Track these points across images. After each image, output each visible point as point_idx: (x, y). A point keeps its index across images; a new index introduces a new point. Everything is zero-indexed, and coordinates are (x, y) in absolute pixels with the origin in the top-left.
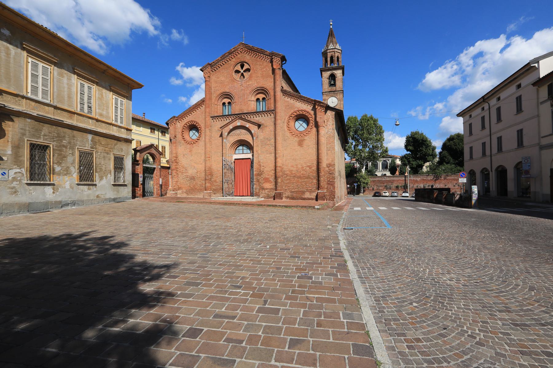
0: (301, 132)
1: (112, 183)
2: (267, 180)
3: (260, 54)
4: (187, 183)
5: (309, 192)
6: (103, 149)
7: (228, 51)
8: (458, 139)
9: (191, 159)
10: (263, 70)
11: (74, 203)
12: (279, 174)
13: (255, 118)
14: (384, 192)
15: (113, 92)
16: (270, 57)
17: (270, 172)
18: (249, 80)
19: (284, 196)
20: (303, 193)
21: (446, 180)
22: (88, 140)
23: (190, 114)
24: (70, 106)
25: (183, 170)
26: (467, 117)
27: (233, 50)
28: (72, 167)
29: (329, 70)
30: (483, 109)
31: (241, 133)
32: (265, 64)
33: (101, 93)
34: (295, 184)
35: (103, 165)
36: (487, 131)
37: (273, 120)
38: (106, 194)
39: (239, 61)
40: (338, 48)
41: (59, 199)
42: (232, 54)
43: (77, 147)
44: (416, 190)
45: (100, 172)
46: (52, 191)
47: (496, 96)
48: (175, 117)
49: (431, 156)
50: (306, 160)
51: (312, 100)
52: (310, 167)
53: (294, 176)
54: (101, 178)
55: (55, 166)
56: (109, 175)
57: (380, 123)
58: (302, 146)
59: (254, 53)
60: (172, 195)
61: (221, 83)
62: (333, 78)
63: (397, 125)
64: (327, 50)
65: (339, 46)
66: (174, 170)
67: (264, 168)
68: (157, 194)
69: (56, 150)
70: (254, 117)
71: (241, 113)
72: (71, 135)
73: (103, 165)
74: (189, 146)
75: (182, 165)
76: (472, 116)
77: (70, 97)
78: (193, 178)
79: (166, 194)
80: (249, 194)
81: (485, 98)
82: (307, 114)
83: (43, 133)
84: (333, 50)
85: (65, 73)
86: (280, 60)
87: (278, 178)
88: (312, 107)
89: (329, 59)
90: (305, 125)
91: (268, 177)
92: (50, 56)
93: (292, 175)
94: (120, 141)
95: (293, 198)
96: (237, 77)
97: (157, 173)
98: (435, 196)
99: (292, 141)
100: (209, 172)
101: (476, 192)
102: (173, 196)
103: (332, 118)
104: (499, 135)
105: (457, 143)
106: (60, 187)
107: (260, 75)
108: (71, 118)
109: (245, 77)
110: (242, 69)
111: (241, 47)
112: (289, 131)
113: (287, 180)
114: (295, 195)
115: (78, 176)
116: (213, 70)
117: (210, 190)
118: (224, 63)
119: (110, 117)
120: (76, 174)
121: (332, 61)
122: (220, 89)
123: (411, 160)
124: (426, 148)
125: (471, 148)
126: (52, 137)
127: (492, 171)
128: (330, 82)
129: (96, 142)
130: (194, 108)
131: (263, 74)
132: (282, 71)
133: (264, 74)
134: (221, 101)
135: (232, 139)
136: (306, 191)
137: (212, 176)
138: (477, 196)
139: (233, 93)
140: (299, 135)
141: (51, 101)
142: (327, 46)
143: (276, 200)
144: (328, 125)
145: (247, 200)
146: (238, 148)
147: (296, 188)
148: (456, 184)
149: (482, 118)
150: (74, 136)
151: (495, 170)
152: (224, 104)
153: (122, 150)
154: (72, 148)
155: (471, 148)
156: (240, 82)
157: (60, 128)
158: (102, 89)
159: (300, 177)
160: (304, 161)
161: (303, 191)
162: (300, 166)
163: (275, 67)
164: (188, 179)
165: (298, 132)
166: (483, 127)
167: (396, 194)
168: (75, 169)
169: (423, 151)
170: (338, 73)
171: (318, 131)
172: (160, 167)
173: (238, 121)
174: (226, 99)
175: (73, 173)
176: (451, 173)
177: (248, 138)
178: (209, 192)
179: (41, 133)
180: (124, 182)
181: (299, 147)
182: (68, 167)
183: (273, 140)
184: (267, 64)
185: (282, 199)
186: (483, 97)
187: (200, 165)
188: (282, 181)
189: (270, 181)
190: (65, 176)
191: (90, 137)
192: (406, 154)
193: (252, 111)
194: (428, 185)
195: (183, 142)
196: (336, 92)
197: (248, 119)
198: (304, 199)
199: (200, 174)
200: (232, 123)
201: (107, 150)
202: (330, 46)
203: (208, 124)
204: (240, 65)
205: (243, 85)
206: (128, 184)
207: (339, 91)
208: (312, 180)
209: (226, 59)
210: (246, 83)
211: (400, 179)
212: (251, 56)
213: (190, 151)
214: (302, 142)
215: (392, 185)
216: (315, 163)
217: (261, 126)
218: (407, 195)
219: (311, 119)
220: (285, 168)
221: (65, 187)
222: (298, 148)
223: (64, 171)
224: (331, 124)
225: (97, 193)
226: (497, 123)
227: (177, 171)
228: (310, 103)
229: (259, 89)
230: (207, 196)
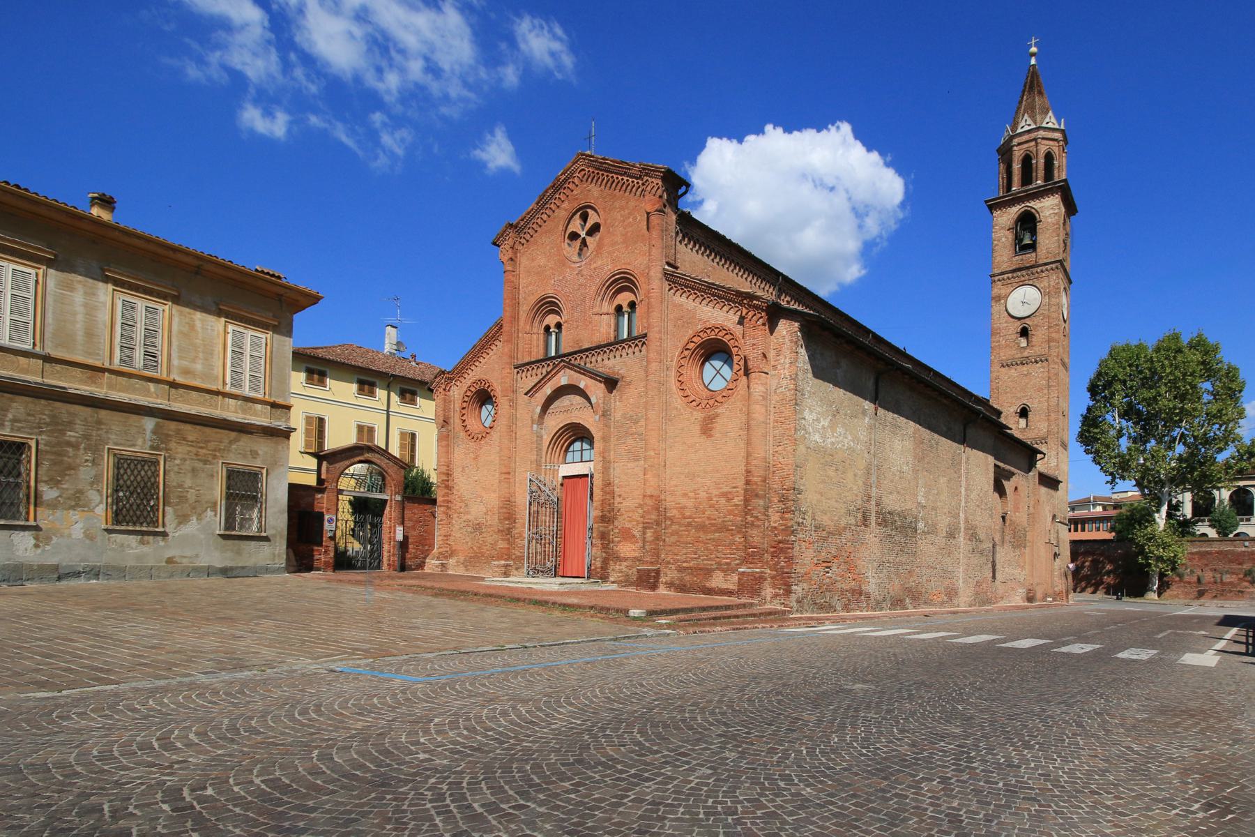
1: (218, 532)
4: (468, 539)
5: (723, 571)
6: (190, 451)
7: (550, 184)
9: (476, 479)
11: (95, 573)
13: (606, 361)
15: (226, 317)
17: (633, 511)
19: (663, 579)
20: (708, 572)
22: (142, 431)
24: (90, 354)
28: (91, 491)
29: (1015, 201)
33: (187, 320)
35: (191, 488)
38: (197, 556)
39: (576, 205)
41: (53, 561)
43: (107, 447)
45: (178, 504)
46: (33, 542)
48: (443, 372)
52: (727, 496)
53: (689, 524)
54: (183, 519)
55: (43, 488)
56: (210, 513)
57: (1227, 356)
58: (711, 436)
61: (538, 273)
64: (1012, 138)
65: (1053, 120)
69: (47, 452)
72: (90, 419)
73: (191, 488)
74: (473, 445)
77: (90, 334)
79: (421, 565)
83: (10, 416)
84: (1033, 135)
85: (80, 282)
86: (660, 183)
89: (1017, 167)
91: (630, 526)
92: (34, 246)
94: (251, 433)
96: (571, 250)
102: (438, 571)
106: (54, 534)
107: (619, 239)
108: (93, 381)
111: (581, 164)
112: (681, 393)
113: (672, 535)
115: (110, 514)
118: (545, 217)
119: (217, 377)
120: (103, 506)
126: (35, 425)
128: (1018, 239)
129: (168, 435)
132: (674, 217)
133: (629, 234)
134: (541, 322)
135: (553, 423)
141: (34, 344)
142: (1014, 128)
144: (779, 367)
145: (546, 588)
150: (99, 422)
153: (254, 454)
154: (95, 449)
157: (58, 404)
158: (192, 311)
159: (702, 527)
160: (714, 480)
161: (707, 569)
168: (101, 495)
170: (1049, 208)
175: (93, 505)
179: (6, 416)
180: (260, 529)
182: (81, 492)
189: (634, 536)
190: (71, 512)
191: (149, 423)
195: (462, 434)
196: (1034, 270)
198: (710, 591)
201: (205, 455)
202: (1023, 123)
204: (581, 216)
205: (584, 273)
206: (274, 536)
207: (1046, 264)
208: (732, 535)
210: (590, 264)
212: (603, 187)
213: (476, 458)
214: (712, 423)
221: (70, 536)
223: (69, 498)
225: (169, 554)
228: (734, 302)
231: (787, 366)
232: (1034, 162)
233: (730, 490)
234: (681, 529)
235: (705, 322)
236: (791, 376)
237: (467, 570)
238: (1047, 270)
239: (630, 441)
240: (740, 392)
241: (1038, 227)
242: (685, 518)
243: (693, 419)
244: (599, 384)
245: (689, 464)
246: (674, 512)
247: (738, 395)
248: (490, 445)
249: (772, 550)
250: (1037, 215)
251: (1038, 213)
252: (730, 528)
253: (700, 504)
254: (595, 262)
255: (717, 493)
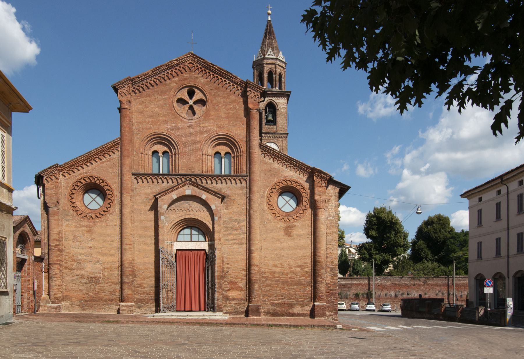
0: (288, 214)
2: (233, 286)
3: (223, 80)
4: (82, 288)
5: (300, 304)
8: (439, 224)
9: (91, 245)
10: (228, 107)
12: (256, 276)
13: (214, 185)
14: (339, 304)
16: (241, 87)
18: (203, 120)
20: (292, 306)
21: (426, 286)
23: (89, 164)
25: (72, 265)
26: (476, 200)
27: (176, 62)
30: (499, 192)
31: (191, 207)
32: (232, 97)
34: (279, 293)
36: (503, 223)
37: (245, 190)
39: (186, 83)
40: (281, 59)
42: (174, 70)
44: (405, 301)
47: (518, 178)
49: (401, 247)
50: (296, 256)
51: (308, 167)
52: (302, 268)
53: (278, 281)
58: (291, 236)
59: (213, 75)
60: (50, 311)
62: (272, 110)
63: (418, 213)
64: (264, 59)
65: (282, 56)
66: (55, 264)
67: (229, 266)
68: (29, 309)
70: (212, 183)
71: (191, 173)
74: (85, 222)
75: (71, 255)
76: (483, 200)
78: (94, 280)
80: (202, 308)
81: (504, 179)
82: (298, 188)
84: (274, 61)
86: (259, 95)
87: (255, 283)
88: (307, 176)
89: (266, 76)
90: (293, 203)
91: (236, 281)
93: (274, 279)
95: (275, 314)
96: (183, 110)
97: (28, 269)
98: (442, 310)
99: (276, 226)
100: (129, 269)
101: (512, 306)
102: (53, 311)
103: (335, 196)
104: (519, 230)
105: (438, 230)
109: (197, 114)
110: (191, 98)
112: (270, 211)
113: (266, 286)
114: (278, 309)
116: (137, 91)
117: (131, 302)
121: (271, 79)
122: (151, 128)
123: (373, 252)
124: (396, 234)
125: (480, 244)
127: (508, 277)
130: (97, 154)
131: (229, 113)
133: (230, 115)
134: (151, 147)
136: (295, 302)
137: (135, 277)
138: (512, 311)
139: (176, 136)
140: (286, 218)
142: (263, 52)
143: (251, 318)
144: (329, 207)
146: (183, 231)
147: (280, 299)
148: (439, 291)
149: (497, 204)
151: (513, 276)
152: (155, 153)
155: (480, 244)
156: (188, 121)
159: (286, 283)
162: (286, 266)
163: (250, 106)
164: (84, 281)
165: (284, 214)
166: (498, 217)
167: (357, 306)
169: (391, 238)
170: (281, 102)
171: (315, 215)
172: (33, 258)
173: (186, 187)
174: (159, 145)
176: (433, 275)
177: (204, 217)
178: (130, 304)
181: (285, 237)
183: (244, 224)
184: (236, 99)
185: (259, 315)
186: (501, 177)
187: (110, 258)
188: (260, 287)
189: (240, 287)
192: (366, 243)
193: (209, 173)
194: (401, 292)
196: (276, 135)
197: (203, 185)
198: (293, 315)
199: (108, 272)
200: (175, 190)
202: (269, 53)
203: (129, 186)
208: (304, 287)
209: (161, 75)
211: (361, 282)
214: (291, 229)
215: (349, 291)
216: (309, 261)
217: (226, 200)
218: (373, 307)
219: (304, 195)
220: (264, 268)
222: (285, 237)
224: (333, 205)
226: (517, 215)
227: (61, 265)
228: (304, 170)
229: (222, 138)
230: (126, 312)
231: (333, 207)
232: (274, 76)
233: (303, 264)
234: (273, 283)
235: (286, 177)
236: (335, 212)
237: (84, 310)
238: (282, 137)
239: (235, 233)
240: (308, 216)
241: (277, 113)
242: (274, 277)
243: (279, 226)
244: (217, 199)
245: (276, 249)
246: (268, 274)
247: (306, 217)
248: (107, 224)
249: (327, 294)
250: (277, 106)
251: (277, 105)
252: (303, 283)
253: (284, 270)
254: (204, 123)
255: (295, 265)
